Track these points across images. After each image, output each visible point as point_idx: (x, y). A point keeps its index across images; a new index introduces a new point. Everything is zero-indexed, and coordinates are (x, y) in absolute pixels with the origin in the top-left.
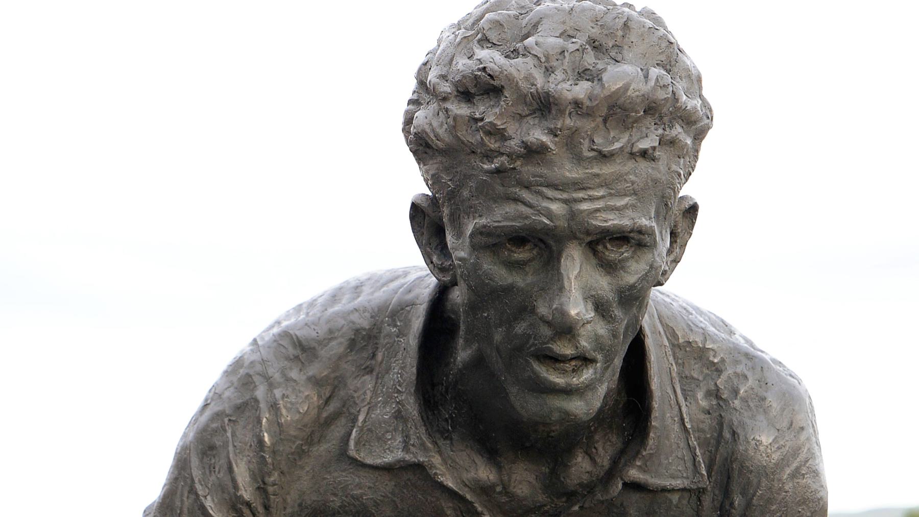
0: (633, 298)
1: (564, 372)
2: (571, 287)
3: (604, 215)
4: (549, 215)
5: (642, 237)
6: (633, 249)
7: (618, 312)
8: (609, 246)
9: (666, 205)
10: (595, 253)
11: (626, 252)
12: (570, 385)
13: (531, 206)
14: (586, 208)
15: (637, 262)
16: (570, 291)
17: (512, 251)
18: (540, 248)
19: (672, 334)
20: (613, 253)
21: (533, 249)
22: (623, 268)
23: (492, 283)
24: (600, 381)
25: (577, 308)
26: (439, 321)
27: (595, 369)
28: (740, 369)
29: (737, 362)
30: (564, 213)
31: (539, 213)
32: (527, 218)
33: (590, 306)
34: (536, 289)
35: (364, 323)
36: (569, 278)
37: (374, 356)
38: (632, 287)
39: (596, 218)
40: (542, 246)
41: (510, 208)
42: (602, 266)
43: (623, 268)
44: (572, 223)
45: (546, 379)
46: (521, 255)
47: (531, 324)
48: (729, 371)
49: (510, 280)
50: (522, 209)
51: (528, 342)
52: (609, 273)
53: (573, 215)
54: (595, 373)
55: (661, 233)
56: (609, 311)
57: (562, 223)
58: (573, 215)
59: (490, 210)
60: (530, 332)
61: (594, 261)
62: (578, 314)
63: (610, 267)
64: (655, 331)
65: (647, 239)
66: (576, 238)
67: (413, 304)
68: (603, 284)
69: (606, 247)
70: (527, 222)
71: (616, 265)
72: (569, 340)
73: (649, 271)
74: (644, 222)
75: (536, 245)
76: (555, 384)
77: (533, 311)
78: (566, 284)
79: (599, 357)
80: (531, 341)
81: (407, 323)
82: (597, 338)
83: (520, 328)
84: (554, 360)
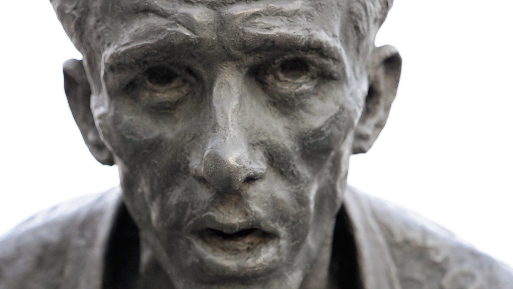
0: (321, 151)
1: (236, 251)
2: (226, 123)
3: (266, 21)
4: (189, 23)
5: (325, 61)
6: (315, 82)
7: (302, 169)
8: (281, 76)
9: (357, 28)
10: (263, 85)
11: (305, 85)
12: (244, 268)
13: (164, 15)
14: (239, 12)
15: (322, 99)
16: (226, 128)
17: (155, 91)
18: (192, 85)
19: (387, 231)
20: (288, 86)
21: (182, 86)
22: (302, 106)
23: (134, 138)
24: (289, 265)
25: (236, 153)
26: (125, 227)
27: (279, 247)
28: (467, 267)
29: (461, 261)
30: (211, 20)
31: (177, 22)
32: (161, 31)
33: (259, 154)
34: (188, 138)
35: (53, 237)
36: (223, 112)
37: (61, 273)
38: (318, 132)
39: (254, 25)
40: (193, 80)
41: (140, 25)
42: (274, 104)
43: (302, 106)
44: (222, 34)
45: (211, 262)
46: (165, 95)
47: (187, 189)
48: (454, 270)
49: (156, 133)
50: (154, 21)
51: (184, 214)
52: (285, 114)
53: (222, 23)
54: (279, 253)
55: (354, 69)
56: (289, 165)
57: (208, 35)
58: (222, 23)
59: (116, 33)
60: (185, 199)
61: (264, 98)
62: (238, 160)
63: (285, 105)
64: (368, 228)
65: (334, 67)
66: (232, 58)
67: (100, 213)
68: (279, 130)
69: (277, 78)
70: (161, 37)
71: (292, 100)
72: (236, 205)
73: (339, 113)
74: (323, 37)
75: (185, 81)
76: (224, 269)
77: (187, 170)
78: (220, 121)
79: (282, 231)
80: (189, 212)
81: (94, 233)
82: (275, 204)
83: (175, 196)
84: (222, 236)
